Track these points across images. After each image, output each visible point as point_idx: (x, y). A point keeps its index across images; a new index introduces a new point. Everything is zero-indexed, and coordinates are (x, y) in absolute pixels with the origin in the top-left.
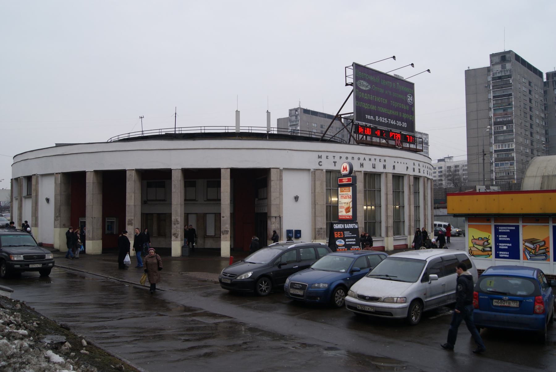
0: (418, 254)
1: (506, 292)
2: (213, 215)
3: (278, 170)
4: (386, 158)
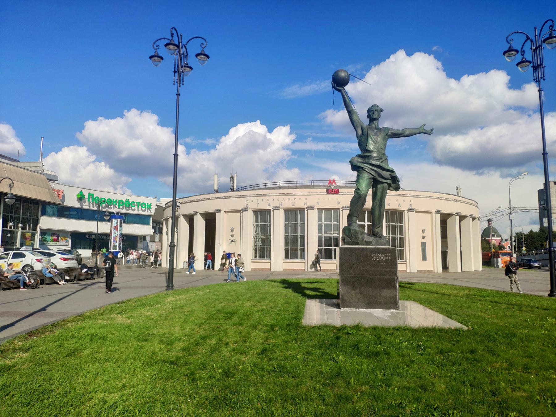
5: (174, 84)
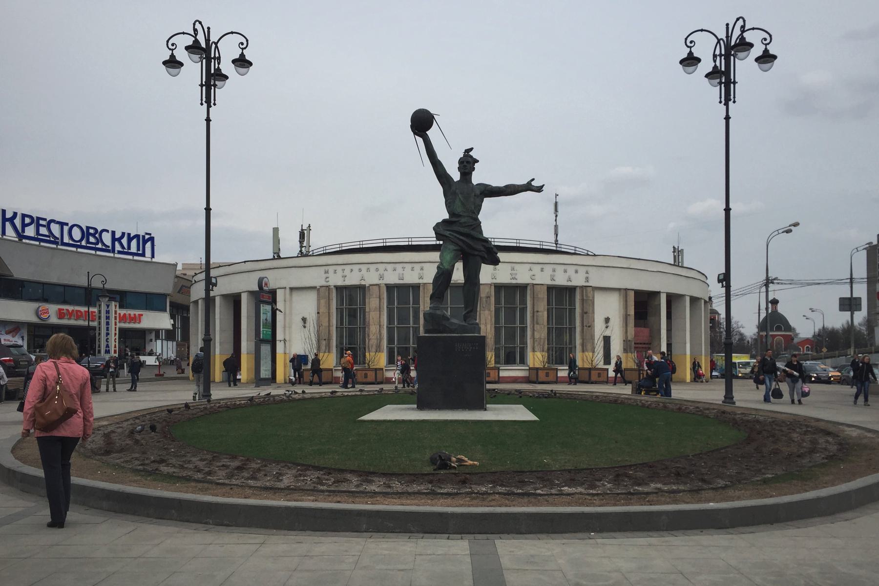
1: (553, 227)
2: (312, 296)
4: (590, 269)
5: (202, 104)
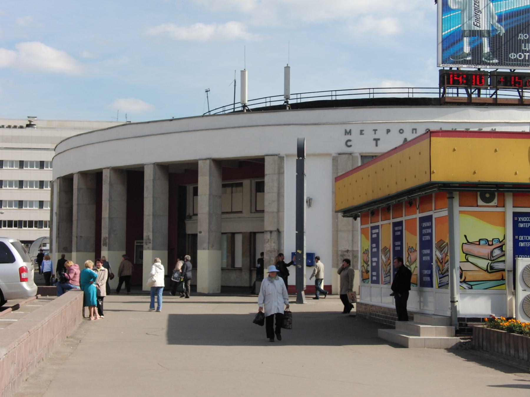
0: (521, 285)
3: (276, 158)
